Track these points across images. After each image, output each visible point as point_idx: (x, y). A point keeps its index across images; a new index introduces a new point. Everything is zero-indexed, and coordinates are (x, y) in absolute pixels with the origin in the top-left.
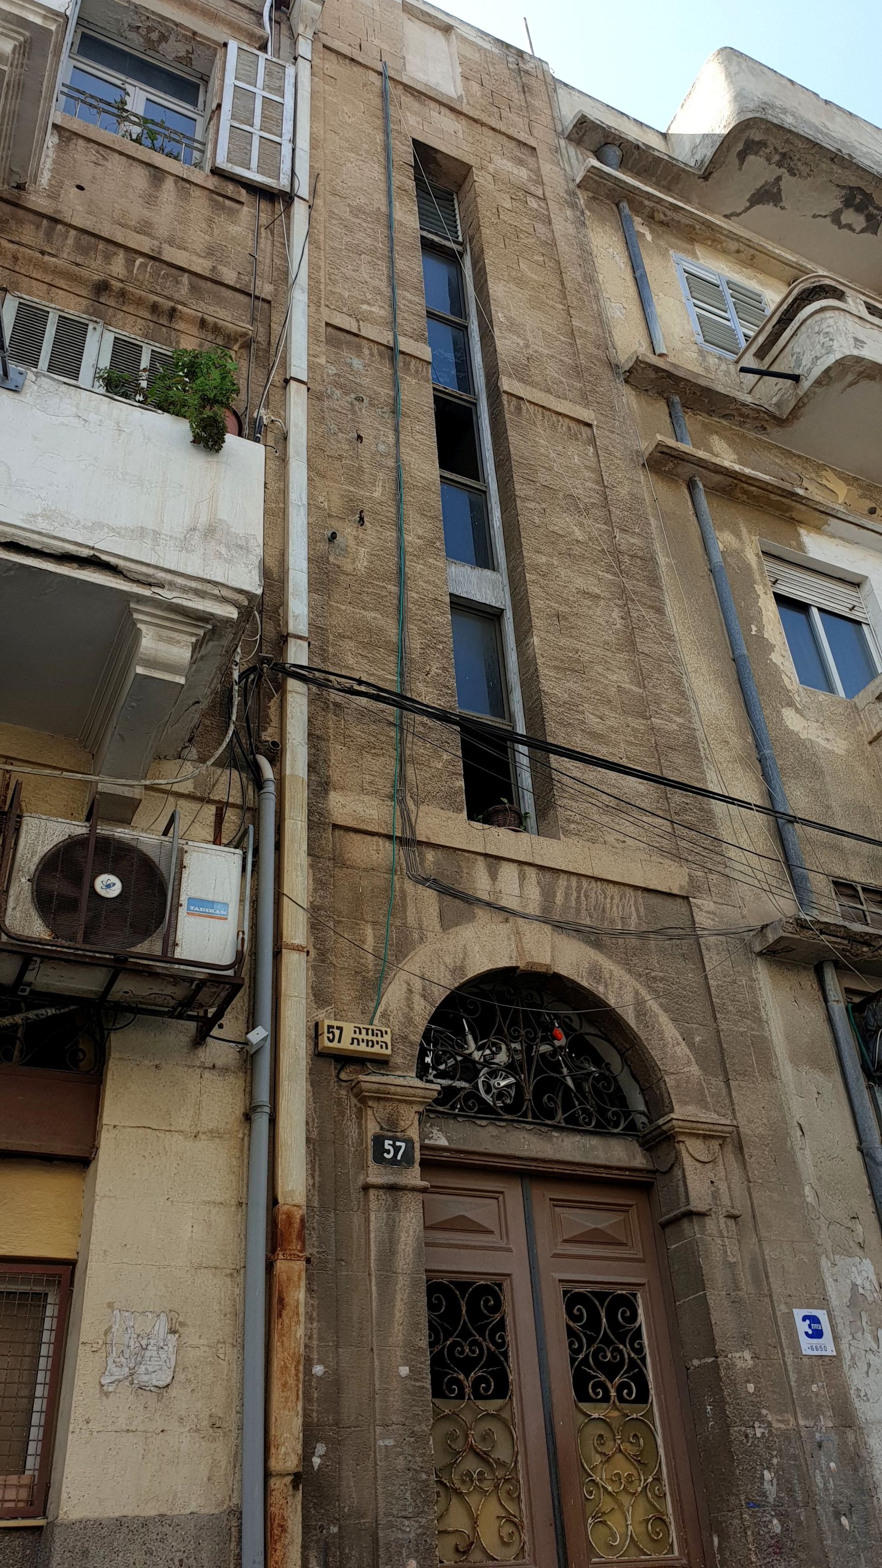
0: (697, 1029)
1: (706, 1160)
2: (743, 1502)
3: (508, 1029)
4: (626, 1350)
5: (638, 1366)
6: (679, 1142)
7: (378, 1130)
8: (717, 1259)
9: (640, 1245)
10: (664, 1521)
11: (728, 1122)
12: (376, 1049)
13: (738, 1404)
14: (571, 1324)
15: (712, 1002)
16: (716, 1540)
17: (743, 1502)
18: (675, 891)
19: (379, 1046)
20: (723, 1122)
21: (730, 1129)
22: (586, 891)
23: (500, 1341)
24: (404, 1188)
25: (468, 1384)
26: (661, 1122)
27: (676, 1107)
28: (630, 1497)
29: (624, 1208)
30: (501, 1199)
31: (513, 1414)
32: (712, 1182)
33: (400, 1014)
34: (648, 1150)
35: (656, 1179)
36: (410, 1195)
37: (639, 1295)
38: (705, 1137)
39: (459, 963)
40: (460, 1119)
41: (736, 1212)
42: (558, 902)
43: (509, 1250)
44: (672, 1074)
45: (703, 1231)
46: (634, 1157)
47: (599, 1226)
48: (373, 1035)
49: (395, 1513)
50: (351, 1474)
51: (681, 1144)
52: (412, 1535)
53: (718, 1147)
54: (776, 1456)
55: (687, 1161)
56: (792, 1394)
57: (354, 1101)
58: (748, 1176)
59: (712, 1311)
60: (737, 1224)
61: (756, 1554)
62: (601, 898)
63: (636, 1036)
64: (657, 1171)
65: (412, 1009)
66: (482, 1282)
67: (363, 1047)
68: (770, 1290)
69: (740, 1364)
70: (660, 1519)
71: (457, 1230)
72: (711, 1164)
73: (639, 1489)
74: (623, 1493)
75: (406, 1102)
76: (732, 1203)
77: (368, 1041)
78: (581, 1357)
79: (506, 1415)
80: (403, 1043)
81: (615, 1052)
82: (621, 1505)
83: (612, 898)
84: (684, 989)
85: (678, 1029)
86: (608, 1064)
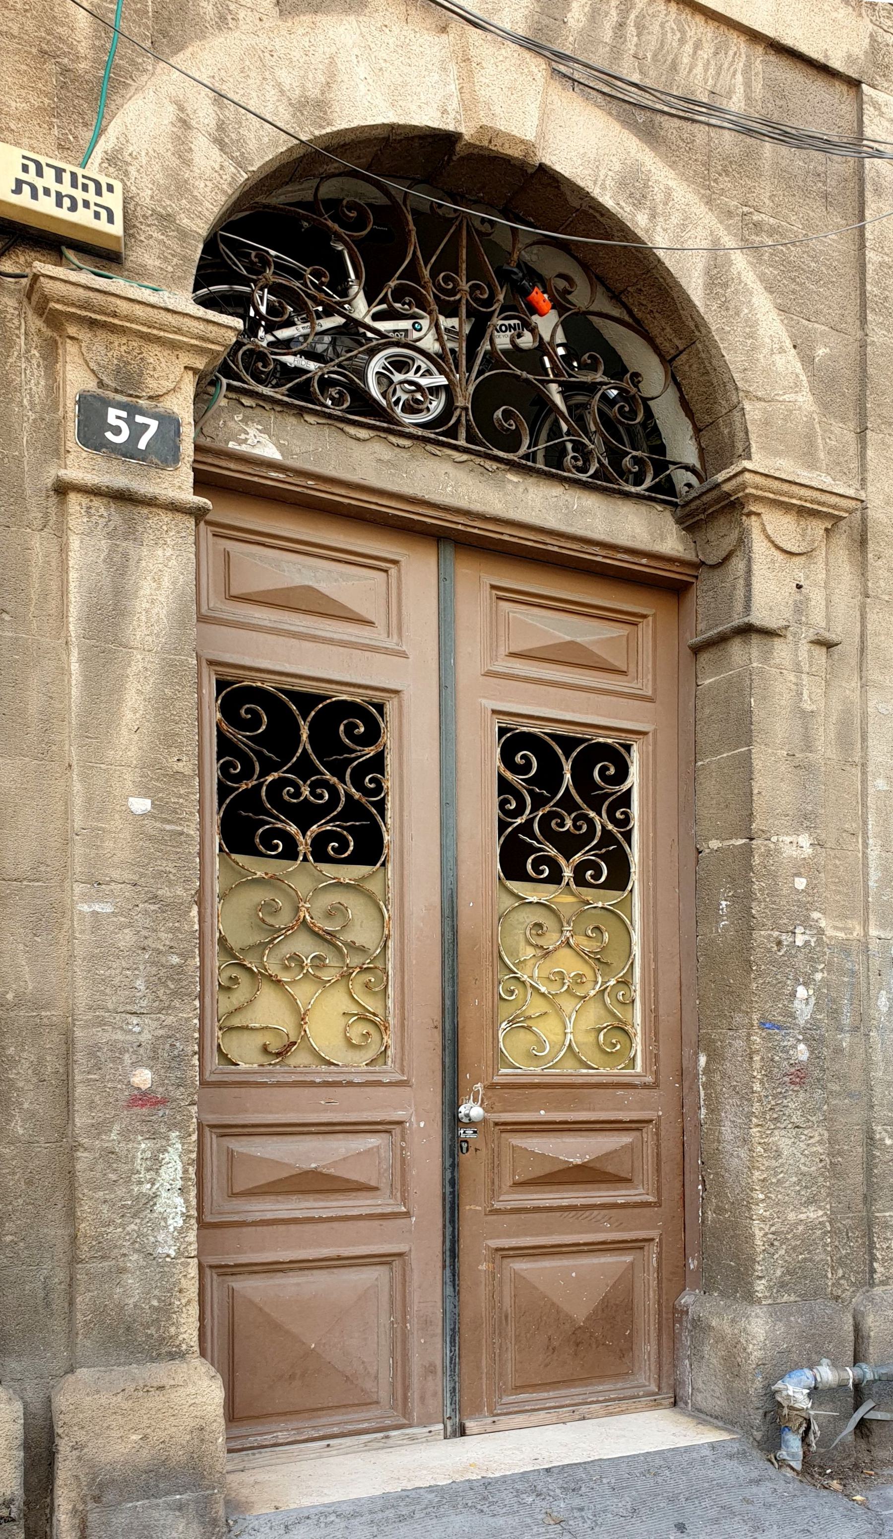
0: (822, 334)
1: (794, 549)
2: (755, 1022)
3: (434, 275)
4: (601, 821)
5: (617, 842)
6: (750, 514)
7: (91, 385)
8: (783, 703)
9: (650, 677)
10: (626, 1032)
11: (851, 492)
12: (83, 217)
13: (774, 903)
14: (509, 775)
15: (863, 293)
16: (703, 1060)
17: (755, 1022)
18: (836, 64)
19: (90, 213)
20: (841, 491)
21: (852, 504)
22: (641, 17)
23: (372, 786)
24: (151, 502)
25: (304, 843)
26: (721, 477)
27: (755, 456)
28: (577, 1000)
29: (631, 620)
30: (393, 571)
31: (386, 887)
32: (799, 587)
33: (157, 168)
34: (689, 529)
35: (697, 577)
36: (166, 517)
37: (635, 748)
38: (803, 512)
39: (314, 92)
40: (311, 419)
41: (832, 637)
42: (571, 22)
43: (403, 655)
44: (759, 399)
45: (766, 657)
46: (663, 538)
47: (578, 640)
48: (74, 185)
49: (110, 1006)
50: (21, 947)
51: (753, 518)
52: (146, 1037)
53: (822, 532)
54: (822, 971)
55: (759, 546)
56: (867, 895)
57: (36, 323)
58: (865, 586)
59: (756, 775)
60: (829, 656)
61: (762, 1083)
62: (673, 39)
63: (700, 324)
64: (703, 563)
65: (188, 163)
66: (344, 697)
67: (46, 206)
68: (865, 757)
69: (789, 851)
70: (621, 1029)
71: (296, 610)
72: (803, 558)
73: (592, 993)
74: (567, 996)
75: (158, 340)
76: (828, 623)
77: (59, 195)
78: (519, 821)
79: (374, 886)
80: (164, 230)
81: (655, 360)
82: (559, 1010)
83: (698, 46)
84: (814, 258)
85: (789, 327)
86: (636, 375)
